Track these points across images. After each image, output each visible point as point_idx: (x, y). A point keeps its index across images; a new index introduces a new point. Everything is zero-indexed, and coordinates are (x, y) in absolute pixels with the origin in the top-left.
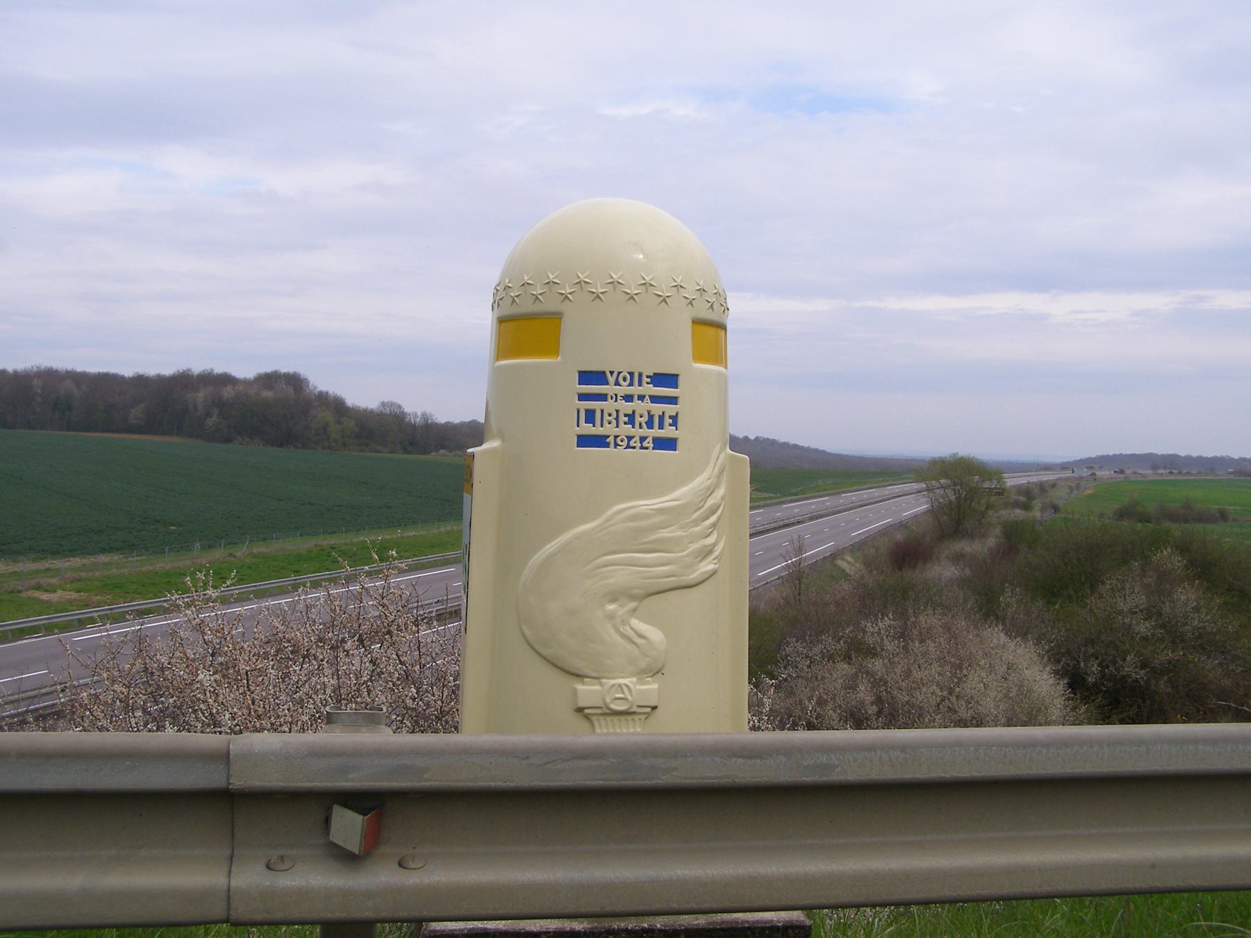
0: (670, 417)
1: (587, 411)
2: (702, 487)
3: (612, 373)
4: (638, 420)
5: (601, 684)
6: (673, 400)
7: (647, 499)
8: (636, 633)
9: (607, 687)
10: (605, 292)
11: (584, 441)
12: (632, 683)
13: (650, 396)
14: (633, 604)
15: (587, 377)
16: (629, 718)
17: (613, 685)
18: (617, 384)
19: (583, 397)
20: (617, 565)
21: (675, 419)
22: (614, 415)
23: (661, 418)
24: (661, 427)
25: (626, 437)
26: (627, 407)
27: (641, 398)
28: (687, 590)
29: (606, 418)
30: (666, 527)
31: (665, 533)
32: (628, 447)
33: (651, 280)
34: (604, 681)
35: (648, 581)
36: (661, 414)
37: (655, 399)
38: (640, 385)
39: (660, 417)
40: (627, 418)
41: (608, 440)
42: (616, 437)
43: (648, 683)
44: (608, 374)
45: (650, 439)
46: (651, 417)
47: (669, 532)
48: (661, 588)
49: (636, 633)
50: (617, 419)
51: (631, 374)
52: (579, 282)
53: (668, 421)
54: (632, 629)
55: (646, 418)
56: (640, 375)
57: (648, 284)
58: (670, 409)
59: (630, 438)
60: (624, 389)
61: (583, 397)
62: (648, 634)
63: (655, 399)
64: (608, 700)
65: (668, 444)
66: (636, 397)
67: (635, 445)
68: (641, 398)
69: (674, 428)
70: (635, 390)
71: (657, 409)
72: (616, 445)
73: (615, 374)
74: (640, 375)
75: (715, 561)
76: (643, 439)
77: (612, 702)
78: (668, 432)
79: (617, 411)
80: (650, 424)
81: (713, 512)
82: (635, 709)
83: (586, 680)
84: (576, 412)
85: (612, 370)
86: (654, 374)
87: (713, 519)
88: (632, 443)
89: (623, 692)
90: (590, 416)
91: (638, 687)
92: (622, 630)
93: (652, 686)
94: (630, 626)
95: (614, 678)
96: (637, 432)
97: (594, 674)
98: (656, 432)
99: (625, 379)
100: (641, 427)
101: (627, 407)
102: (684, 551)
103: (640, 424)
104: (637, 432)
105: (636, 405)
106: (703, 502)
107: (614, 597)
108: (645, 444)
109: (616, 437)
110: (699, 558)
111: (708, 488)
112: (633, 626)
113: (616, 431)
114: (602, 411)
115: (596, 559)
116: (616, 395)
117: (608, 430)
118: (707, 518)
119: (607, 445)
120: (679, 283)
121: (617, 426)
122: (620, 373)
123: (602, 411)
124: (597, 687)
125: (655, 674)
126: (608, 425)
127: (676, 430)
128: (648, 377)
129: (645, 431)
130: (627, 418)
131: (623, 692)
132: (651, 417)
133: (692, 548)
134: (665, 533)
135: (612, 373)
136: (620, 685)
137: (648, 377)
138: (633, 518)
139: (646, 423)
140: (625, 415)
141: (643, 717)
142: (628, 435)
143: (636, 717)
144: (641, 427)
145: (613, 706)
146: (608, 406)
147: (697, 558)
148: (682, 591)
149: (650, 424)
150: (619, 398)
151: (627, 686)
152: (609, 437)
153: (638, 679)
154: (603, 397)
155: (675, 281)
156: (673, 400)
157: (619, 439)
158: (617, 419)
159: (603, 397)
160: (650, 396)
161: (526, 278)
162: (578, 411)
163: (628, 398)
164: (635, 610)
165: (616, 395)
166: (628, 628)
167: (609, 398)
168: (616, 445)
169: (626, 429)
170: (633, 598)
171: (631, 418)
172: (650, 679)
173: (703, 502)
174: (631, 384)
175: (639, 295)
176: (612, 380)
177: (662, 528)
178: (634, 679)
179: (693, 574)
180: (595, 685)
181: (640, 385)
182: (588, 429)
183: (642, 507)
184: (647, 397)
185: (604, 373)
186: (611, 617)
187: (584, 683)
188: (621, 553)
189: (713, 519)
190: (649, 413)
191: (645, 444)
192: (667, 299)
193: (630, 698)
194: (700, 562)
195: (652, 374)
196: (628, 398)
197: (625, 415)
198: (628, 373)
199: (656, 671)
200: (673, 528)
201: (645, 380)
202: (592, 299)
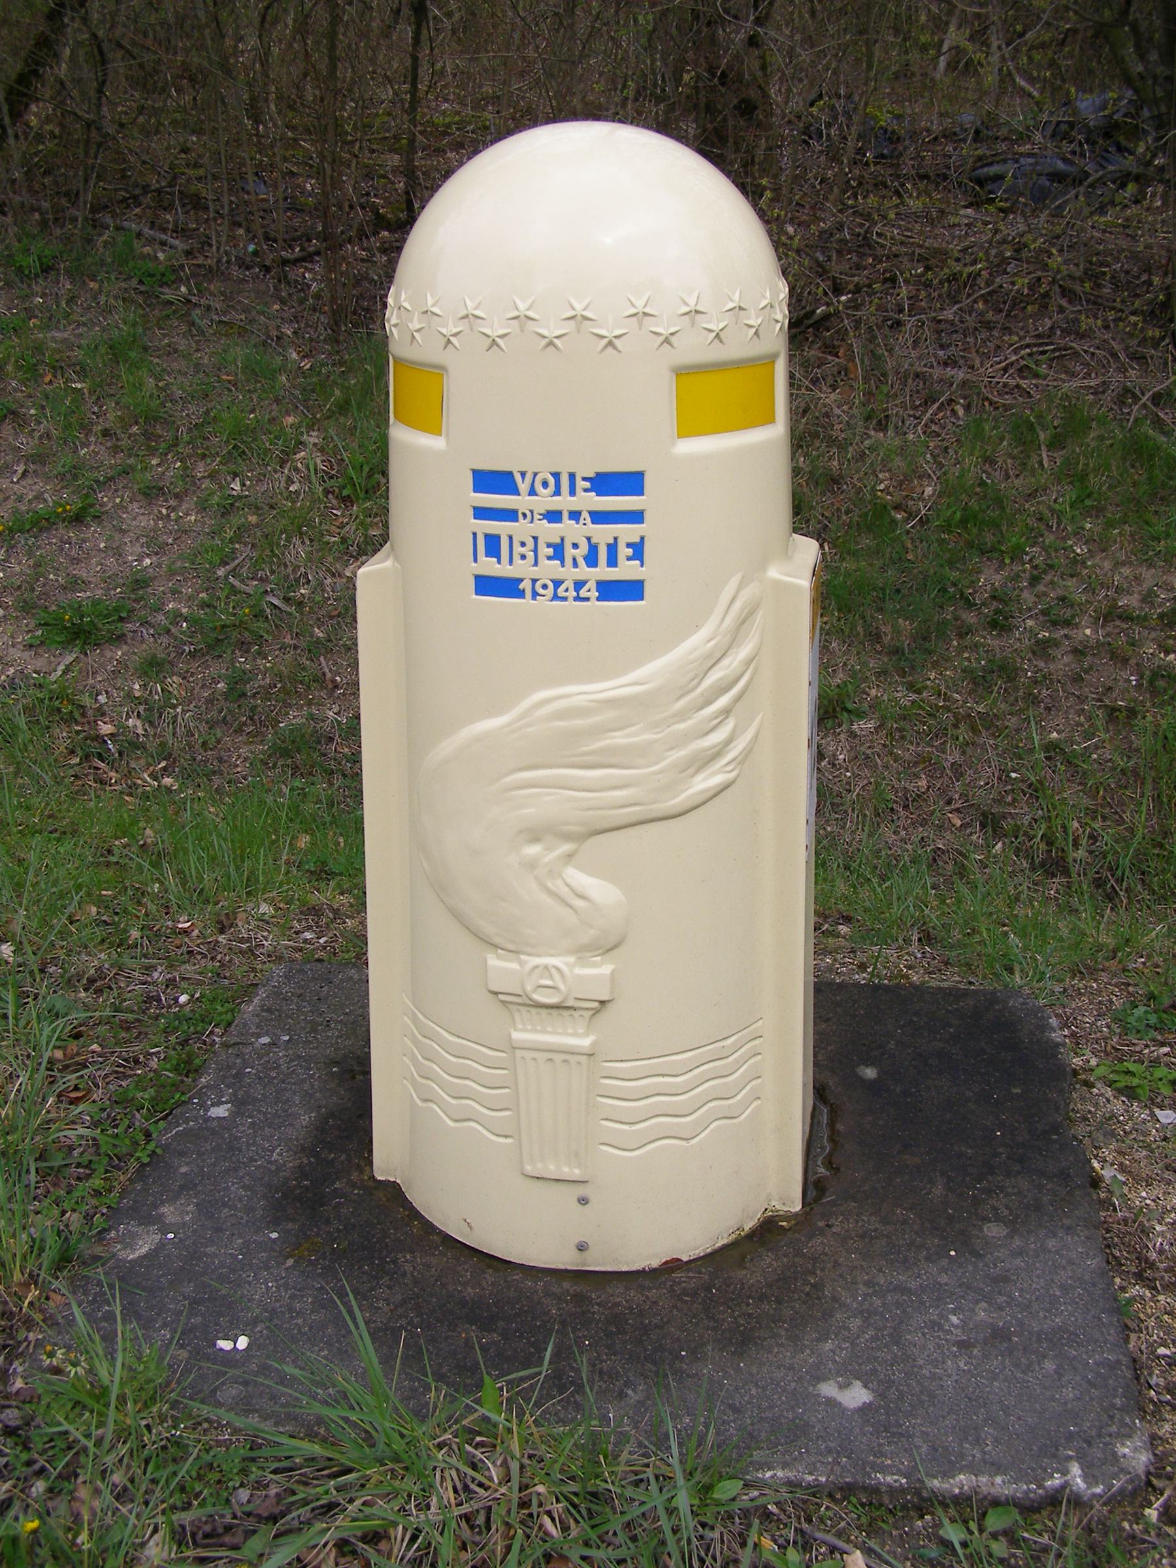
0: (629, 545)
1: (487, 536)
2: (692, 657)
3: (523, 474)
4: (569, 552)
5: (521, 963)
6: (636, 517)
7: (590, 681)
8: (572, 890)
9: (528, 967)
10: (505, 335)
11: (487, 585)
12: (566, 964)
13: (590, 513)
14: (567, 847)
15: (487, 480)
16: (566, 1013)
17: (537, 967)
18: (532, 492)
19: (481, 513)
20: (533, 786)
21: (638, 550)
22: (530, 544)
23: (612, 548)
24: (612, 562)
25: (552, 581)
26: (550, 532)
27: (575, 515)
28: (671, 821)
29: (518, 549)
30: (619, 729)
31: (619, 739)
32: (556, 597)
33: (585, 309)
34: (522, 957)
35: (591, 813)
36: (612, 541)
37: (599, 517)
38: (572, 492)
39: (609, 545)
40: (551, 550)
41: (521, 587)
42: (534, 581)
43: (595, 965)
44: (518, 478)
45: (592, 584)
46: (593, 548)
47: (629, 736)
48: (615, 824)
49: (572, 890)
50: (535, 551)
51: (556, 475)
52: (466, 317)
53: (624, 552)
54: (568, 885)
55: (584, 549)
56: (572, 476)
57: (579, 317)
58: (627, 532)
59: (557, 583)
60: (545, 501)
61: (481, 513)
62: (594, 894)
63: (599, 517)
64: (529, 988)
65: (632, 590)
66: (565, 515)
67: (565, 594)
68: (575, 515)
69: (638, 562)
70: (564, 502)
71: (604, 533)
72: (535, 594)
73: (529, 477)
74: (572, 476)
75: (730, 768)
76: (579, 585)
77: (534, 991)
78: (626, 570)
79: (535, 538)
80: (591, 559)
81: (724, 690)
82: (570, 1003)
83: (500, 951)
84: (471, 536)
85: (524, 470)
86: (598, 474)
87: (723, 701)
88: (561, 592)
89: (551, 977)
90: (493, 545)
91: (577, 971)
92: (550, 885)
93: (604, 968)
94: (563, 879)
95: (539, 956)
96: (569, 574)
97: (510, 946)
98: (604, 572)
99: (545, 484)
100: (575, 565)
101: (550, 532)
102: (656, 763)
103: (574, 559)
104: (569, 574)
105: (567, 529)
106: (696, 681)
107: (535, 835)
108: (583, 593)
109: (534, 581)
110: (691, 771)
111: (709, 656)
112: (569, 880)
113: (534, 572)
114: (511, 538)
115: (507, 775)
116: (532, 512)
117: (519, 569)
118: (709, 703)
119: (521, 594)
120: (640, 309)
121: (536, 564)
122: (535, 474)
123: (511, 538)
124: (514, 966)
125: (608, 951)
126: (521, 562)
127: (642, 565)
128: (584, 479)
129: (584, 571)
130: (551, 550)
131: (551, 977)
132: (593, 548)
133: (674, 757)
134: (619, 739)
135: (523, 474)
136: (546, 967)
137: (584, 479)
138: (562, 715)
139: (585, 559)
140: (549, 545)
141: (588, 1014)
142: (554, 577)
143: (576, 1014)
144: (575, 565)
145: (536, 997)
146: (519, 529)
147: (684, 771)
148: (644, 826)
149: (591, 559)
150: (537, 516)
151: (557, 969)
152: (522, 580)
153: (579, 958)
154: (510, 515)
155: (633, 305)
156: (636, 517)
157: (538, 584)
158: (535, 551)
159: (510, 515)
160: (590, 513)
161: (430, 301)
162: (475, 534)
163: (553, 516)
164: (570, 856)
165: (532, 512)
166: (559, 882)
167: (520, 516)
168: (535, 594)
169: (550, 569)
170: (567, 837)
171: (558, 551)
172: (599, 958)
173: (696, 681)
174: (557, 492)
175: (564, 338)
176: (523, 487)
177: (614, 730)
178: (571, 959)
179: (675, 797)
180: (509, 961)
181: (572, 492)
182: (490, 567)
183: (579, 697)
184: (585, 515)
185: (510, 474)
186: (531, 865)
187: (498, 957)
188: (551, 767)
189: (723, 701)
190: (589, 539)
191: (583, 593)
192: (615, 340)
193: (562, 987)
194: (693, 776)
195: (592, 475)
196: (553, 516)
197: (549, 545)
198: (552, 474)
199: (609, 947)
200: (633, 729)
201: (581, 484)
202: (486, 347)
